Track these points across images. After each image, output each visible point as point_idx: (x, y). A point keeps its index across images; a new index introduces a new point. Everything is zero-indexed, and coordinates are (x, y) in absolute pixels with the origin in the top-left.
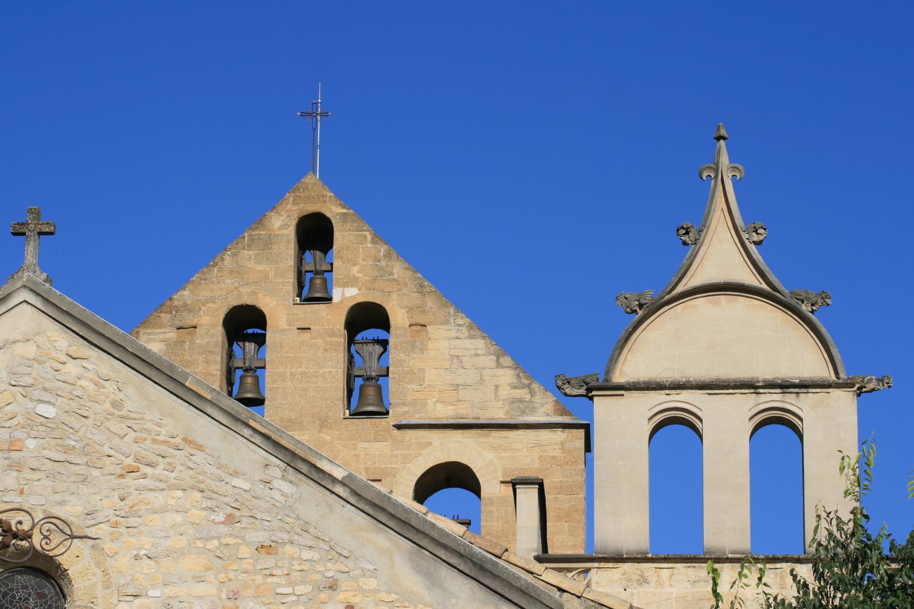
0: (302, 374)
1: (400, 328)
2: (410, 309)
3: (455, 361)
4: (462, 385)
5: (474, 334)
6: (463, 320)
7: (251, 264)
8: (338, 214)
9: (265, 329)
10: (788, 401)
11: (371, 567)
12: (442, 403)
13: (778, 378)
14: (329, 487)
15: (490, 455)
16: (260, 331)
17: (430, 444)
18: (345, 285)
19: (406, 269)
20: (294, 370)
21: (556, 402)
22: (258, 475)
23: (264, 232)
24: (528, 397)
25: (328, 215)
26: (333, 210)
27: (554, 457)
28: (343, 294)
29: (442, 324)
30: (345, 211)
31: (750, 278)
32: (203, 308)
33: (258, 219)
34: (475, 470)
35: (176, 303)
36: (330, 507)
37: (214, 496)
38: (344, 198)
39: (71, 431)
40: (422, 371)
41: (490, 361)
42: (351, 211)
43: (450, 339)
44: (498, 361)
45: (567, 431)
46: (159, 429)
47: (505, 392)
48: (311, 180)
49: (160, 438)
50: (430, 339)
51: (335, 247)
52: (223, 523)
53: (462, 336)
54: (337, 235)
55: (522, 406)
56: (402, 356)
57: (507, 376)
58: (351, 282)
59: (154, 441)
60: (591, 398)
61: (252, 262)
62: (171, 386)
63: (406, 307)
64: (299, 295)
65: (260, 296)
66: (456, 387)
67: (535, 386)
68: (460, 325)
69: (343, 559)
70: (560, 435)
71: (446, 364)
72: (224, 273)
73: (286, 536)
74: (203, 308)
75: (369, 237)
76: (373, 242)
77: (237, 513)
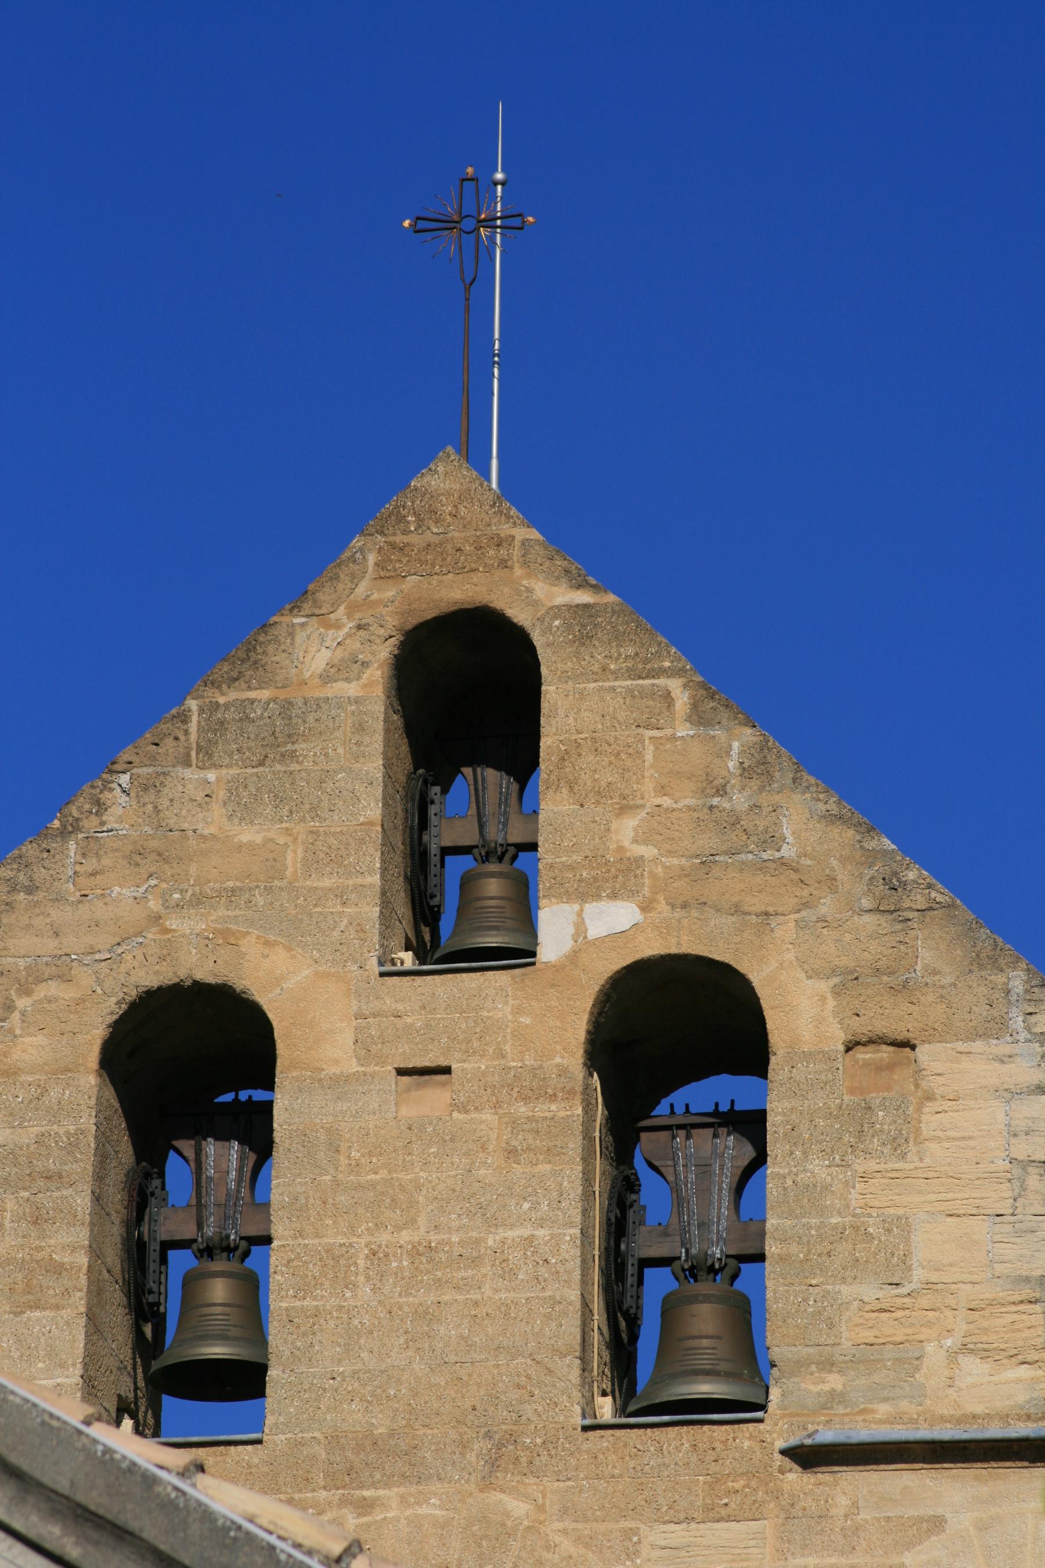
0: (414, 1252)
1: (809, 1056)
8: (557, 611)
12: (985, 1354)
17: (937, 1524)
20: (384, 1237)
23: (264, 694)
28: (580, 928)
30: (584, 597)
42: (611, 598)
43: (1012, 1094)
51: (542, 766)
54: (551, 693)
56: (818, 1169)
65: (250, 945)
71: (998, 1198)
72: (107, 861)
75: (682, 699)
76: (698, 717)
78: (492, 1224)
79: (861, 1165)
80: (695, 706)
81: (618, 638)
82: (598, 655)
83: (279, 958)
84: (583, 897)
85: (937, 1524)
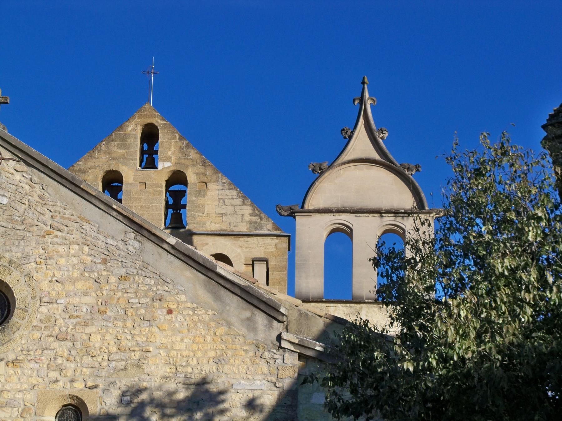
0: (141, 206)
1: (193, 184)
2: (198, 174)
3: (221, 201)
4: (224, 214)
5: (231, 187)
6: (225, 180)
7: (115, 149)
8: (162, 124)
9: (122, 184)
10: (399, 221)
11: (183, 289)
12: (215, 223)
13: (393, 209)
14: (160, 244)
15: (239, 250)
16: (119, 185)
17: (207, 244)
18: (164, 161)
19: (196, 153)
20: (137, 204)
21: (273, 223)
22: (122, 236)
23: (123, 133)
24: (259, 221)
25: (156, 124)
26: (158, 121)
27: (272, 252)
28: (164, 165)
29: (214, 182)
30: (165, 122)
31: (377, 157)
32: (90, 171)
33: (120, 126)
34: (230, 258)
35: (75, 168)
36: (160, 255)
37: (96, 248)
38: (164, 116)
39: (16, 211)
40: (204, 206)
41: (239, 202)
42: (169, 123)
43: (219, 190)
44: (243, 202)
45: (279, 238)
46: (65, 211)
47: (247, 218)
48: (148, 106)
49: (67, 216)
50: (208, 190)
51: (159, 141)
52: (100, 263)
53: (225, 188)
54: (160, 135)
55: (255, 225)
56: (194, 198)
57: (248, 210)
58: (169, 159)
59: (63, 218)
60: (294, 217)
61: (116, 148)
62: (73, 187)
63: (196, 173)
64: (140, 166)
65: (120, 165)
66: (222, 215)
67: (262, 215)
68: (224, 183)
69: (166, 284)
70: (275, 241)
71: (217, 203)
72: (101, 153)
73: (135, 271)
74: (90, 171)
75: (177, 137)
76: (180, 139)
77: (108, 258)
78: (152, 203)
79: (199, 198)
80: (179, 138)
81: (169, 128)
82: (166, 130)
83: (124, 167)
84: (164, 162)
85: (207, 244)
